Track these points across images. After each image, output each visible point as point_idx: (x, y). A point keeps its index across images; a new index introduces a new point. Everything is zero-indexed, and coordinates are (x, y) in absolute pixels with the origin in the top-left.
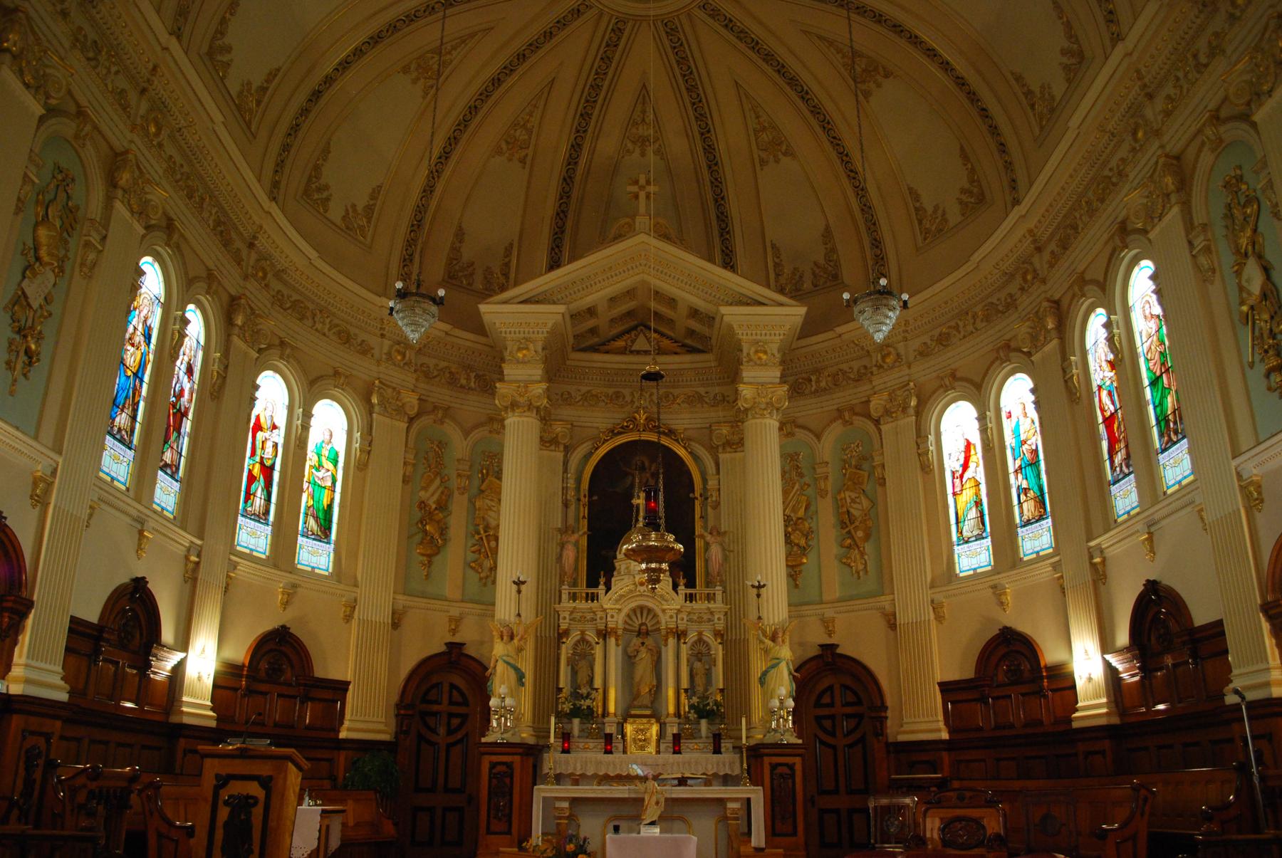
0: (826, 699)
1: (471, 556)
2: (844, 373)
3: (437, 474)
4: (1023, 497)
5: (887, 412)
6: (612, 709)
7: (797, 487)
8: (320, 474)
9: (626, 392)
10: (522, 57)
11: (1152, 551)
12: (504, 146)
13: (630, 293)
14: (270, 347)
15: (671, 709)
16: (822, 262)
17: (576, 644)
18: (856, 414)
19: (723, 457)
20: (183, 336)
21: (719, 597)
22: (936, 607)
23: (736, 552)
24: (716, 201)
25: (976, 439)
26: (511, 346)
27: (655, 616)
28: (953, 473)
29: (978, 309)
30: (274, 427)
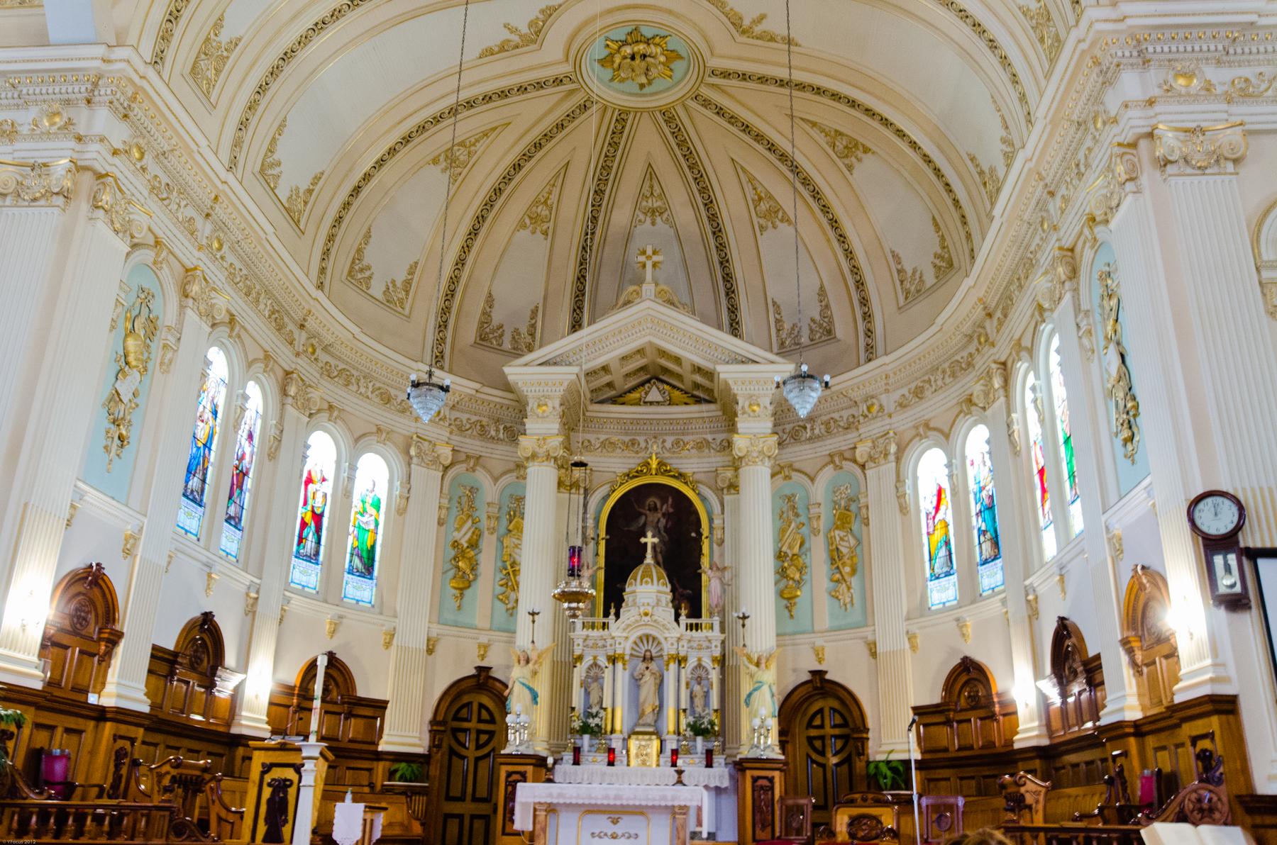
0: (817, 722)
1: (499, 590)
2: (835, 421)
3: (469, 516)
4: (982, 539)
5: (871, 458)
6: (618, 726)
7: (793, 525)
8: (365, 519)
9: (641, 439)
10: (538, 146)
11: (1064, 590)
12: (528, 221)
13: (640, 352)
14: (319, 411)
15: (672, 727)
16: (817, 317)
17: (589, 668)
18: (846, 459)
19: (727, 498)
20: (243, 410)
21: (717, 627)
22: (911, 637)
23: (730, 587)
24: (721, 263)
25: (946, 486)
26: (532, 404)
27: (659, 643)
28: (927, 515)
29: (946, 365)
30: (324, 480)
